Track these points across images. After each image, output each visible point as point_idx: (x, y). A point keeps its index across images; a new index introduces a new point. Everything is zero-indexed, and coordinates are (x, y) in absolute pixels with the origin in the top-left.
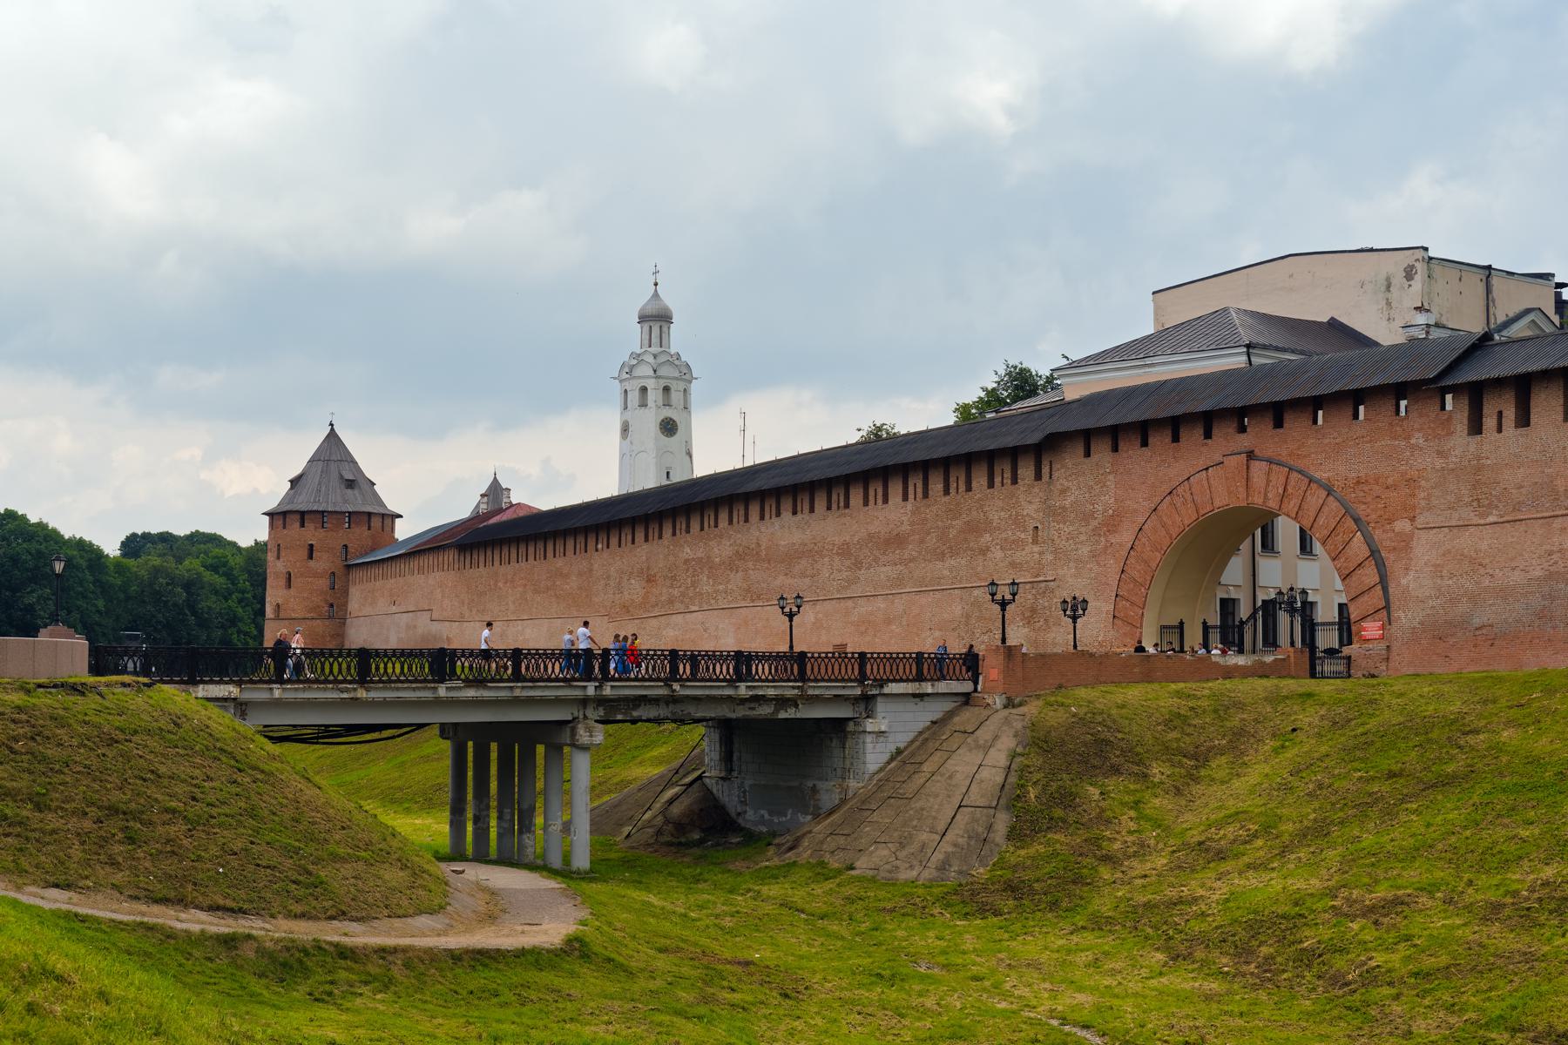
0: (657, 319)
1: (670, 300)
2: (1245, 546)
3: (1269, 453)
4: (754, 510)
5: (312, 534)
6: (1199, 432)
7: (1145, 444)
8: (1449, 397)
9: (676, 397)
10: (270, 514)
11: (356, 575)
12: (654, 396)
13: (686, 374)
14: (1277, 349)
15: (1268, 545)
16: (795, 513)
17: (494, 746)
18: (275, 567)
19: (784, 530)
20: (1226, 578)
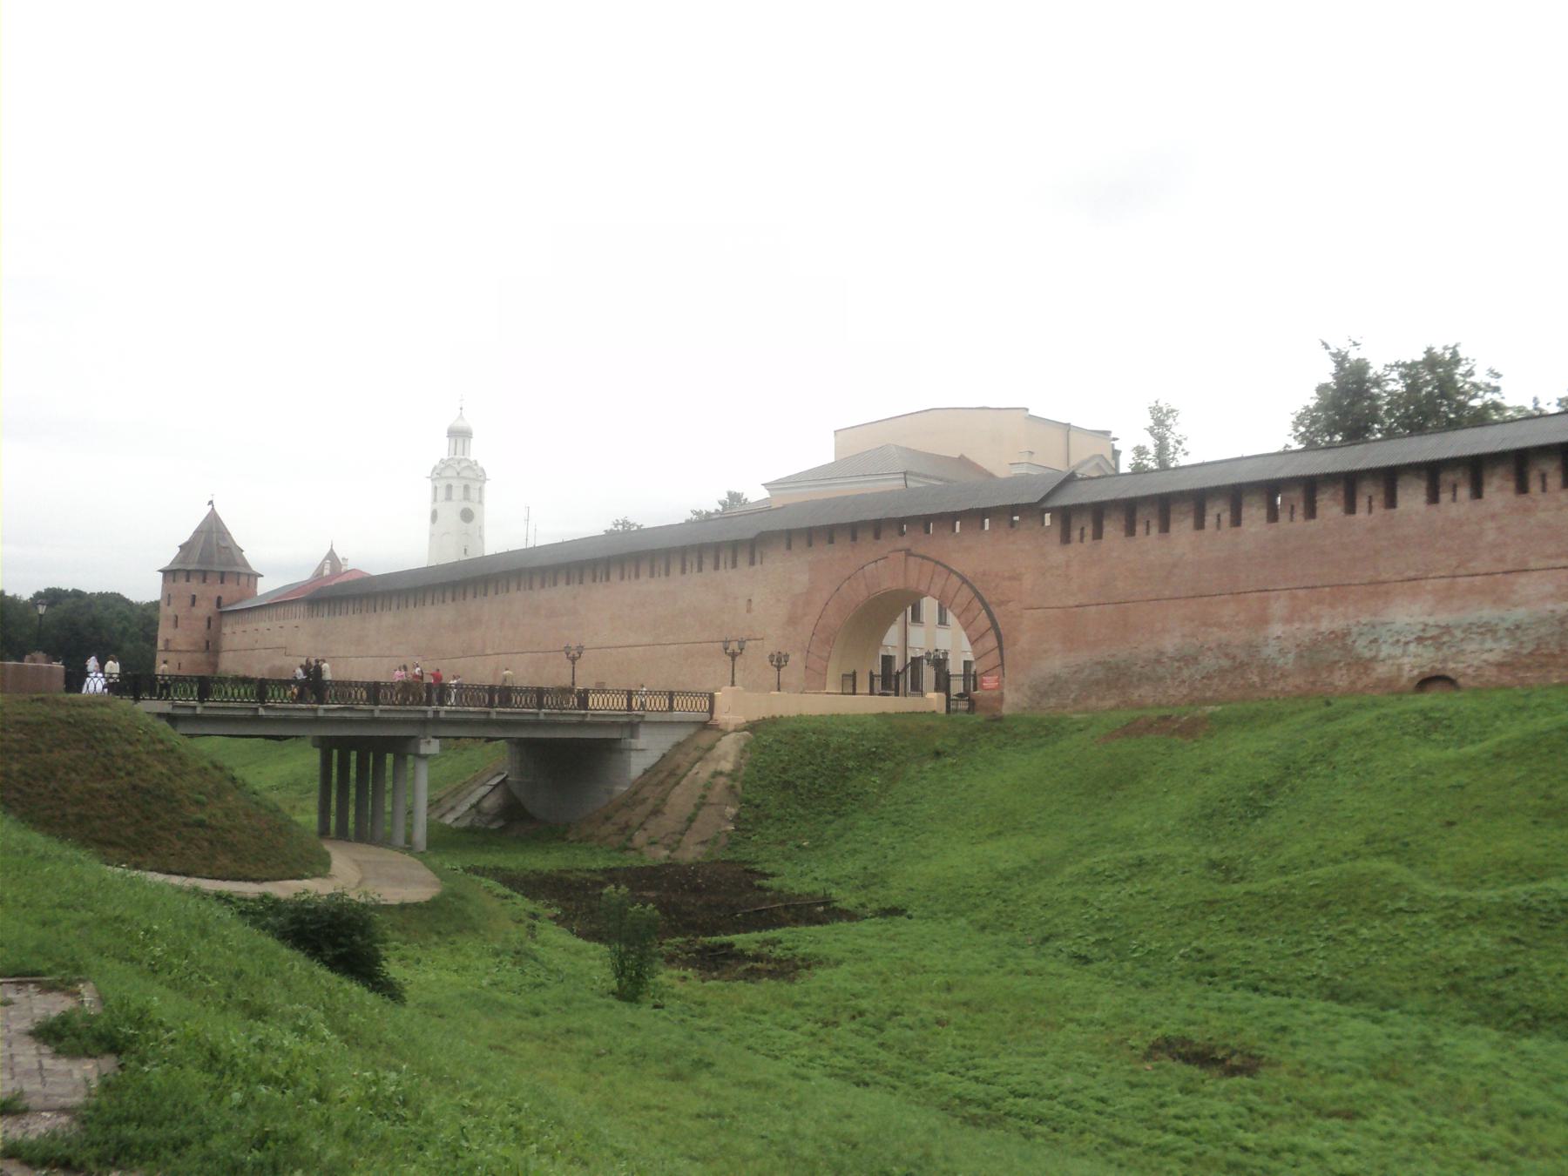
0: (459, 435)
1: (470, 422)
2: (900, 619)
3: (922, 551)
4: (449, 595)
5: (195, 587)
6: (870, 536)
7: (789, 547)
8: (1047, 516)
9: (474, 494)
10: (165, 572)
11: (229, 620)
12: (458, 493)
13: (481, 477)
14: (926, 477)
15: (916, 617)
16: (652, 575)
17: (335, 752)
18: (166, 612)
19: (560, 594)
20: (885, 642)
